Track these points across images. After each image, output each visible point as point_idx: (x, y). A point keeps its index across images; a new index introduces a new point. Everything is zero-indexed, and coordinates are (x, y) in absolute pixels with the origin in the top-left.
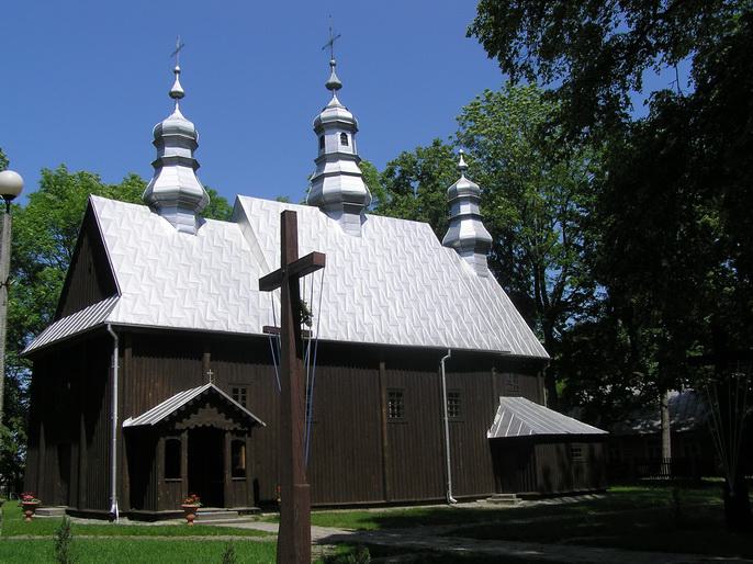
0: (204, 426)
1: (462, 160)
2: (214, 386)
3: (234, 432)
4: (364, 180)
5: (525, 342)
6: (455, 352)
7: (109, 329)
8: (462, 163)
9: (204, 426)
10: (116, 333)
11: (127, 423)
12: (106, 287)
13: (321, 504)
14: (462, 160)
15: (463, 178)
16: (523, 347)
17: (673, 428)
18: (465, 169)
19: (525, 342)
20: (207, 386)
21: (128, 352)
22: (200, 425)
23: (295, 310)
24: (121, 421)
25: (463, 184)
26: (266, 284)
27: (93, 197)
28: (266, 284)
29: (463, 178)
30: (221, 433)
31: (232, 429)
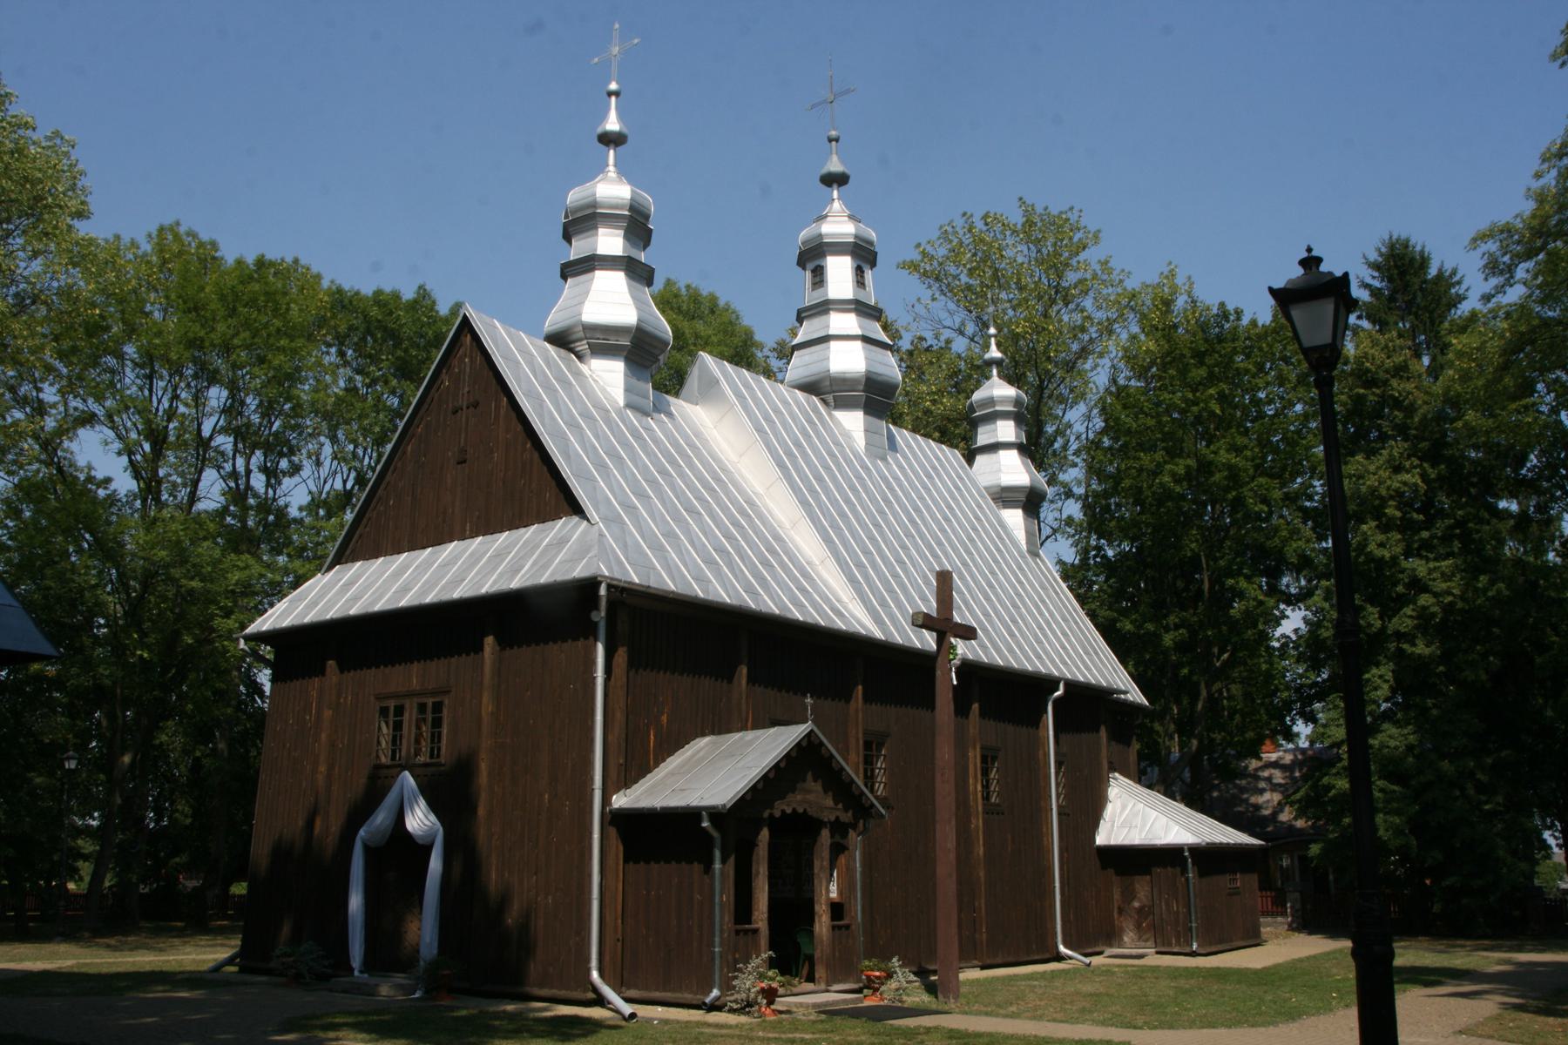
1: (993, 347)
6: (1072, 686)
11: (620, 801)
14: (993, 347)
15: (995, 378)
17: (1184, 870)
21: (621, 656)
22: (801, 810)
24: (606, 800)
29: (995, 378)
31: (833, 819)
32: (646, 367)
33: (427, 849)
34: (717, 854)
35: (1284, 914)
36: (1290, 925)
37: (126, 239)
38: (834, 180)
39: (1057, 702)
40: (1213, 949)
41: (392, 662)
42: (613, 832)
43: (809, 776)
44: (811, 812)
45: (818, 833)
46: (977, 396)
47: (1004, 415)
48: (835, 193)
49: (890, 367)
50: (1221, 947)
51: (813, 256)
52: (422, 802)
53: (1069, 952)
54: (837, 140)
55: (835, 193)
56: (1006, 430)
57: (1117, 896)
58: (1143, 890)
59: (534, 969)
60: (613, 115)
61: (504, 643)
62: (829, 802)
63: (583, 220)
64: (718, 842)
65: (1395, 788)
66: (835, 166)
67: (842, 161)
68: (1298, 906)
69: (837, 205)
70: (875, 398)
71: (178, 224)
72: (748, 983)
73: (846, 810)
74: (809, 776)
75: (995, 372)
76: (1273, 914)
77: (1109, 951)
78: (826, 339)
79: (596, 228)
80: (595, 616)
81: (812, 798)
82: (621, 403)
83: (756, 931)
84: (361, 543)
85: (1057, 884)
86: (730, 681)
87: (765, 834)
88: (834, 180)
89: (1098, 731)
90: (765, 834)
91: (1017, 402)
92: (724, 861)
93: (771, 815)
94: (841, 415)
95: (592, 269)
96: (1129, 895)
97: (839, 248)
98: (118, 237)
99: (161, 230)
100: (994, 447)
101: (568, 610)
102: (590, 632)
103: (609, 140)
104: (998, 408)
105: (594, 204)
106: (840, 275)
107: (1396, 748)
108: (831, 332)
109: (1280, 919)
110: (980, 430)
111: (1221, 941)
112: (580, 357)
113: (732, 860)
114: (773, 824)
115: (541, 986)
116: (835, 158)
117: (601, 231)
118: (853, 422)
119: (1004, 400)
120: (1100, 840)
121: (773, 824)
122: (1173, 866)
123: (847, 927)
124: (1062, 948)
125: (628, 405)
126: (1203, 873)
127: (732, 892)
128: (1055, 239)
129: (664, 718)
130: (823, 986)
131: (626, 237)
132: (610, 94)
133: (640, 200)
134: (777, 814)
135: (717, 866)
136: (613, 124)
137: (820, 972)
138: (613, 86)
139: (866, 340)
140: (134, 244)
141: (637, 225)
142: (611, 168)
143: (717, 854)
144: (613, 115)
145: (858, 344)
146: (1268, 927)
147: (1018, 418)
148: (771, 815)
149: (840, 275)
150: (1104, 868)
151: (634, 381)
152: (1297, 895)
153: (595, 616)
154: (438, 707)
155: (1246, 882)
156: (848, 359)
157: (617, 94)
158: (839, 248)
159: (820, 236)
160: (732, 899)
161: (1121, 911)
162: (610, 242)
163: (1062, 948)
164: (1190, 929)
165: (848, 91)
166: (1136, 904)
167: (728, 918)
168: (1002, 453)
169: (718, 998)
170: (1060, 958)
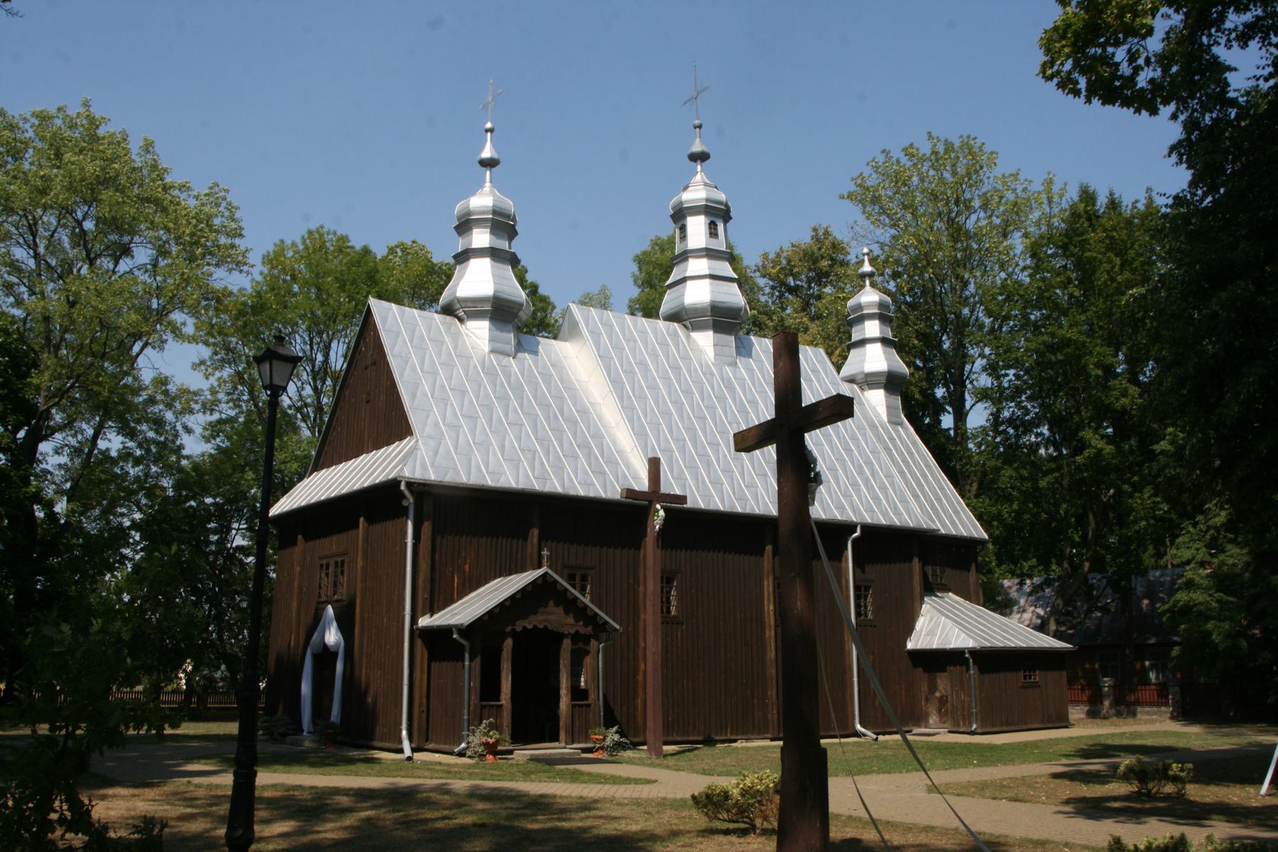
0: (535, 626)
1: (867, 263)
2: (550, 572)
3: (576, 637)
4: (740, 287)
5: (954, 516)
6: (869, 530)
7: (403, 487)
8: (867, 268)
9: (535, 626)
10: (412, 492)
11: (424, 621)
12: (392, 424)
13: (686, 738)
14: (867, 263)
15: (868, 287)
16: (953, 523)
17: (968, 670)
18: (871, 275)
19: (954, 516)
20: (540, 572)
21: (427, 528)
22: (541, 626)
23: (799, 474)
24: (414, 620)
25: (869, 297)
26: (747, 441)
27: (373, 302)
28: (747, 441)
29: (868, 287)
30: (557, 638)
31: (573, 631)
32: (511, 322)
33: (335, 654)
34: (467, 656)
35: (1166, 704)
36: (1172, 713)
37: (288, 242)
38: (701, 157)
39: (854, 541)
40: (990, 730)
41: (325, 536)
42: (419, 642)
43: (551, 603)
44: (550, 627)
45: (561, 642)
46: (850, 303)
47: (871, 317)
48: (699, 168)
49: (734, 296)
50: (1005, 728)
51: (680, 215)
52: (335, 624)
53: (863, 730)
54: (700, 127)
55: (699, 168)
56: (872, 328)
57: (925, 687)
58: (943, 683)
59: (379, 730)
60: (488, 146)
61: (370, 521)
62: (571, 620)
63: (465, 225)
64: (467, 648)
65: (1231, 599)
66: (697, 147)
67: (703, 142)
68: (1178, 698)
69: (698, 177)
70: (722, 319)
71: (322, 227)
72: (477, 739)
73: (586, 625)
74: (551, 603)
75: (868, 282)
76: (1158, 705)
77: (916, 731)
78: (683, 280)
79: (471, 229)
80: (405, 503)
81: (553, 617)
82: (487, 349)
83: (501, 706)
84: (325, 457)
85: (855, 679)
86: (525, 539)
87: (509, 643)
88: (701, 157)
89: (911, 561)
90: (509, 643)
91: (881, 305)
92: (471, 660)
93: (513, 630)
94: (697, 336)
95: (468, 259)
96: (933, 688)
97: (695, 211)
98: (282, 241)
99: (310, 232)
100: (862, 342)
101: (382, 501)
102: (403, 513)
103: (489, 164)
104: (865, 312)
105: (469, 213)
106: (697, 229)
107: (1234, 565)
108: (688, 274)
109: (1163, 709)
110: (854, 330)
111: (1008, 724)
112: (461, 320)
113: (478, 660)
114: (514, 634)
115: (381, 740)
116: (698, 141)
117: (475, 231)
118: (705, 340)
119: (870, 305)
120: (910, 645)
121: (514, 634)
122: (961, 665)
123: (589, 706)
124: (858, 727)
125: (492, 351)
126: (982, 670)
127: (478, 679)
128: (962, 161)
129: (467, 567)
130: (563, 744)
131: (492, 232)
132: (487, 131)
133: (503, 206)
134: (519, 629)
135: (467, 663)
136: (487, 153)
137: (562, 736)
138: (489, 125)
139: (713, 277)
140: (294, 244)
141: (503, 224)
142: (488, 184)
143: (467, 656)
144: (488, 146)
145: (707, 281)
146: (1076, 713)
147: (883, 318)
148: (513, 630)
149: (697, 229)
150: (915, 666)
151: (498, 333)
152: (1177, 688)
153: (405, 503)
154: (343, 562)
155: (1056, 680)
156: (698, 294)
157: (491, 130)
158: (695, 211)
159: (681, 203)
160: (478, 685)
161: (927, 700)
162: (481, 238)
163: (858, 727)
164: (970, 714)
165: (704, 90)
166: (938, 694)
167: (475, 698)
168: (869, 347)
169: (464, 749)
170: (857, 734)
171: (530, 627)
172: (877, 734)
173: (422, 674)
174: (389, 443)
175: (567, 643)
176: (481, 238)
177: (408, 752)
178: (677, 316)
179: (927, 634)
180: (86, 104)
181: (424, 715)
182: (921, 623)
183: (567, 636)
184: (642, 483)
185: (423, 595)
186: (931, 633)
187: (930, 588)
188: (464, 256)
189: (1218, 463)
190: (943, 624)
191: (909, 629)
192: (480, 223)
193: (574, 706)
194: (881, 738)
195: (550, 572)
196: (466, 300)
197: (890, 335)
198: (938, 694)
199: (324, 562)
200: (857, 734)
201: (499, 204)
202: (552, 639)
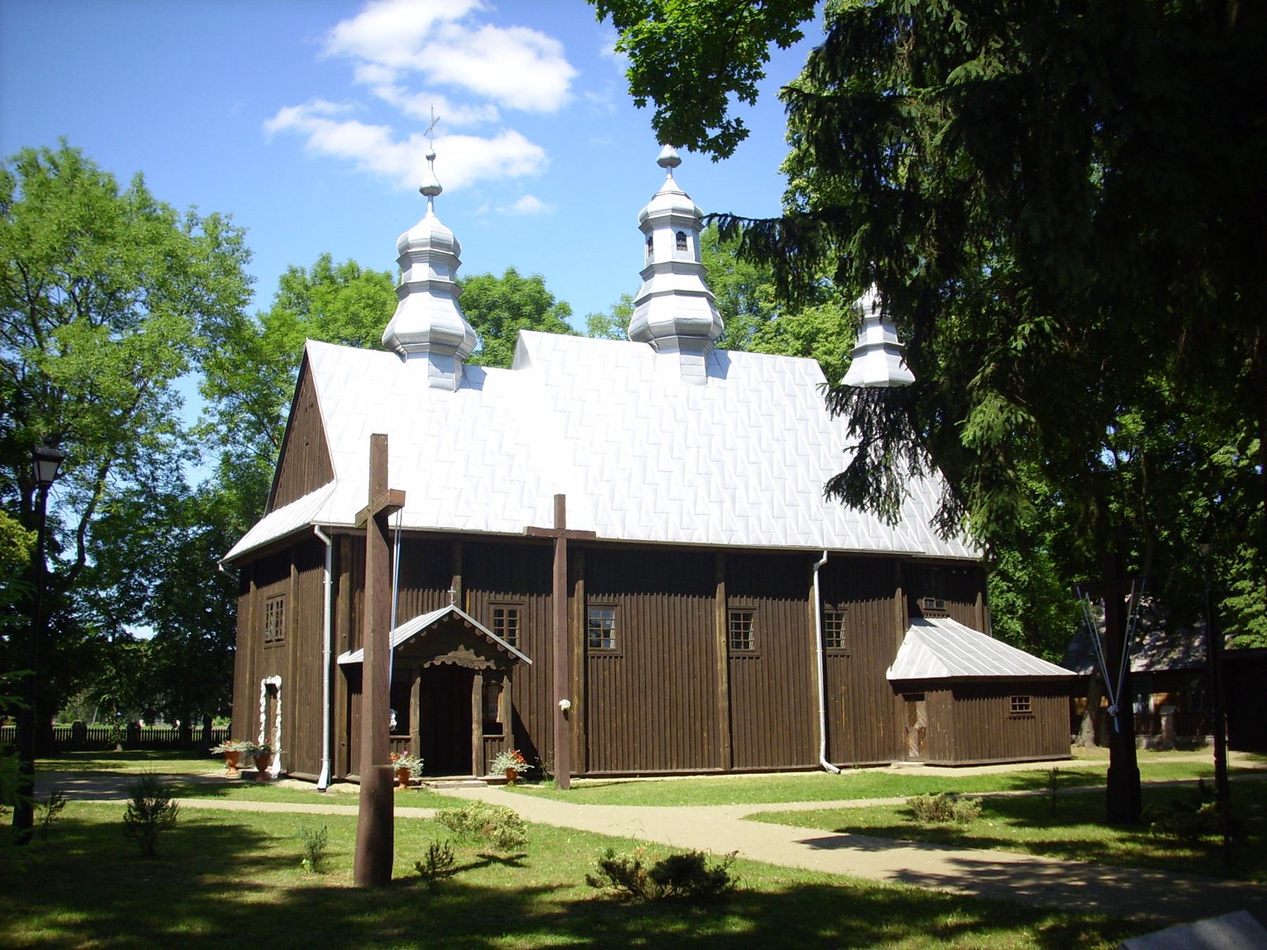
2: (457, 610)
3: (487, 673)
6: (835, 555)
7: (317, 531)
30: (469, 673)
31: (484, 667)
39: (821, 569)
44: (459, 664)
63: (406, 260)
83: (502, 739)
100: (864, 350)
105: (408, 246)
111: (956, 759)
121: (424, 674)
123: (408, 740)
133: (441, 236)
155: (1055, 709)
158: (662, 222)
159: (647, 214)
162: (421, 272)
170: (822, 768)
171: (449, 663)
172: (841, 768)
173: (341, 706)
174: (321, 486)
175: (478, 680)
176: (421, 272)
177: (322, 782)
178: (642, 336)
179: (908, 664)
180: (64, 142)
181: (345, 749)
182: (903, 652)
183: (477, 672)
184: (546, 521)
185: (342, 634)
186: (911, 663)
187: (916, 616)
188: (404, 291)
189: (209, 610)
190: (937, 649)
191: (890, 658)
192: (419, 257)
193: (486, 740)
194: (843, 772)
195: (457, 610)
196: (404, 335)
197: (894, 340)
198: (917, 726)
199: (270, 602)
200: (822, 768)
201: (435, 234)
202: (464, 675)
